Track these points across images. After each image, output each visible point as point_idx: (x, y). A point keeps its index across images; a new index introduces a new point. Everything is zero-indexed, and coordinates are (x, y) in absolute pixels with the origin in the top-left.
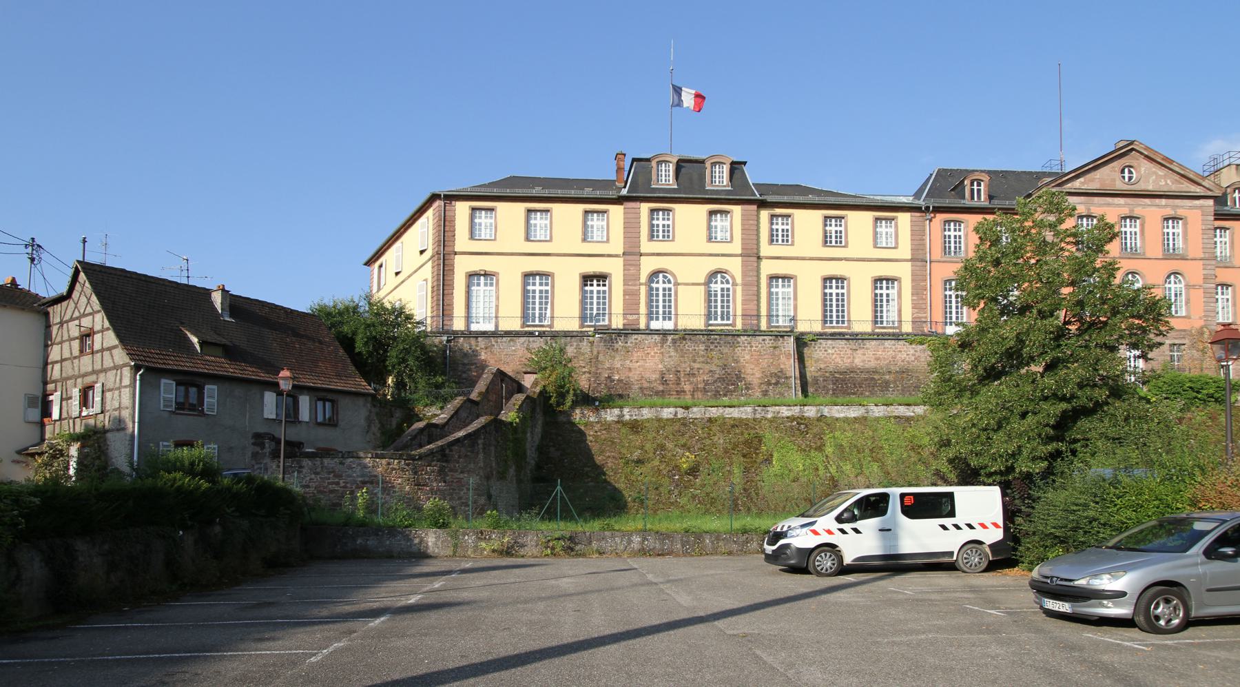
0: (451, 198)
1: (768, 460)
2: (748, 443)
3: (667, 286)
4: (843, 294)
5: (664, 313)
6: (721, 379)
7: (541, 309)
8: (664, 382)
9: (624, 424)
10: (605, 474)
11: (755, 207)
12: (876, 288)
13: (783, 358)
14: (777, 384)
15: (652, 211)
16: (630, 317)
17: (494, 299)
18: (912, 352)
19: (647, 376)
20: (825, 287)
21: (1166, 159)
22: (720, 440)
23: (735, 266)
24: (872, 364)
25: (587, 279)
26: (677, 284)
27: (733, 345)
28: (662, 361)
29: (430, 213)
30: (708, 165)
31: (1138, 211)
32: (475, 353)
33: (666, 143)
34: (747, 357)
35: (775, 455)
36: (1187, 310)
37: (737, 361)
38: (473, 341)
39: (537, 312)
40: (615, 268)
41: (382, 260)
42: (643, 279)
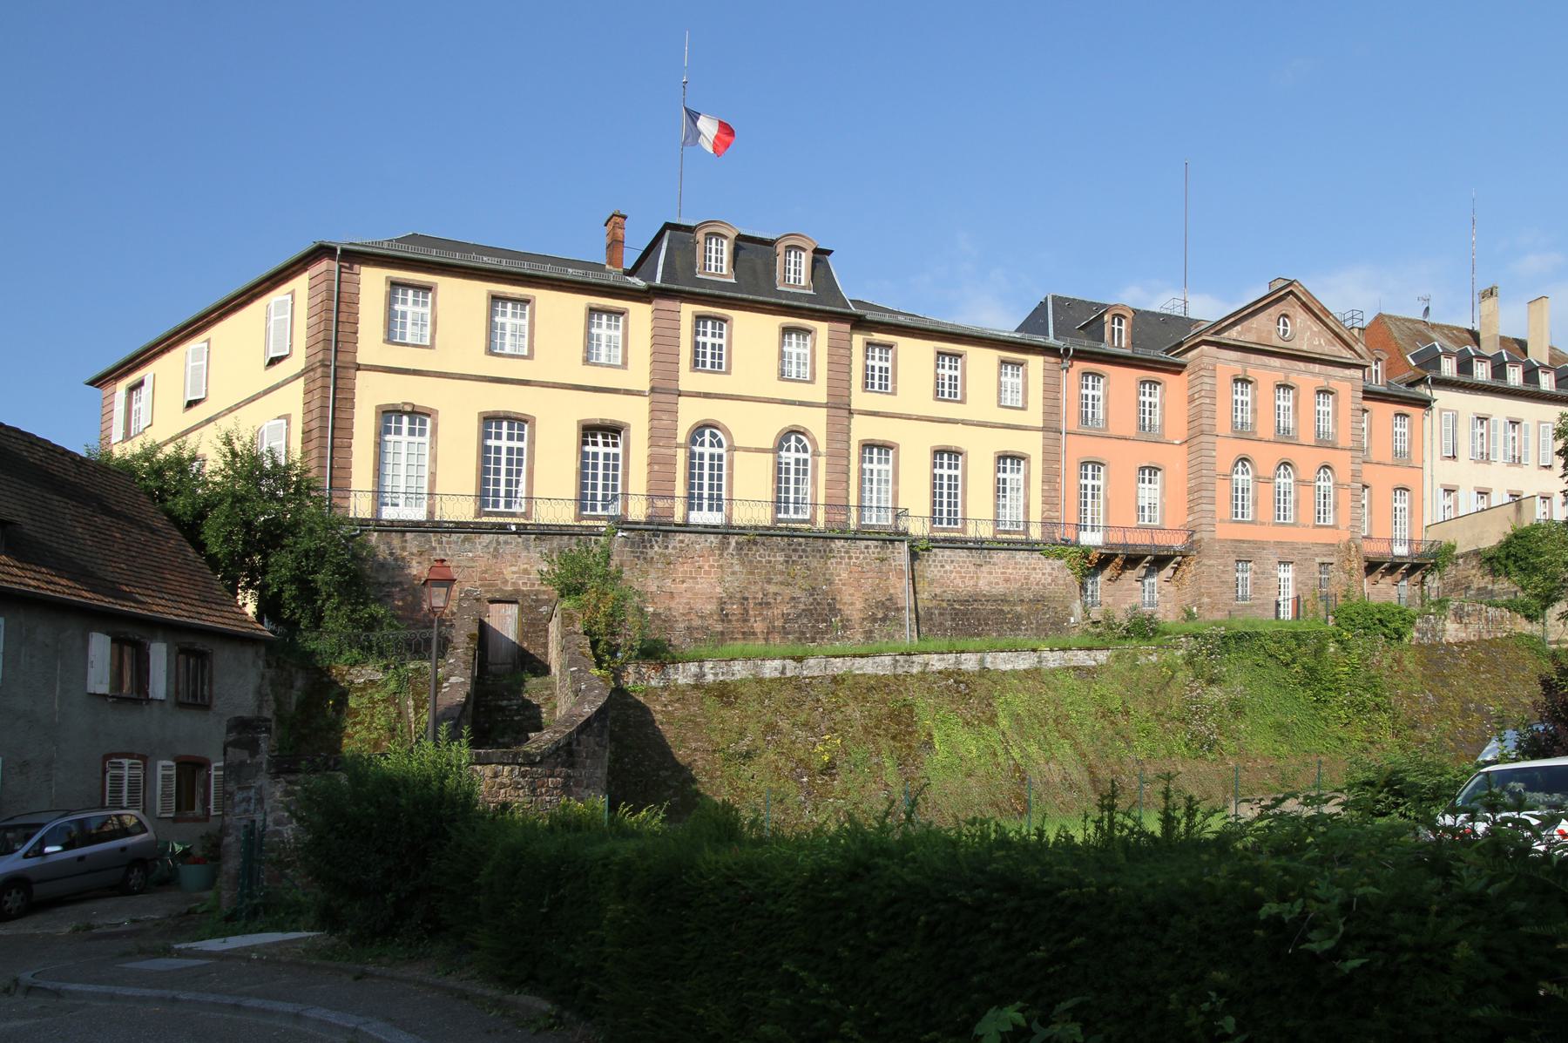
0: (355, 257)
1: (929, 744)
2: (894, 716)
3: (716, 451)
4: (616, 456)
5: (711, 497)
6: (808, 612)
7: (509, 483)
8: (725, 617)
9: (708, 690)
10: (694, 780)
11: (847, 327)
12: (585, 443)
13: (893, 579)
14: (884, 619)
15: (700, 318)
16: (660, 503)
17: (426, 460)
18: (1049, 570)
19: (698, 606)
20: (487, 435)
21: (1324, 310)
22: (854, 711)
23: (816, 422)
24: (1000, 589)
25: (589, 431)
26: (732, 449)
27: (826, 555)
28: (721, 581)
29: (301, 283)
30: (780, 249)
31: (1293, 379)
32: (400, 564)
33: (728, 205)
34: (844, 575)
35: (935, 733)
36: (1336, 518)
37: (830, 582)
38: (396, 540)
39: (503, 488)
40: (635, 414)
41: (146, 372)
42: (682, 437)
